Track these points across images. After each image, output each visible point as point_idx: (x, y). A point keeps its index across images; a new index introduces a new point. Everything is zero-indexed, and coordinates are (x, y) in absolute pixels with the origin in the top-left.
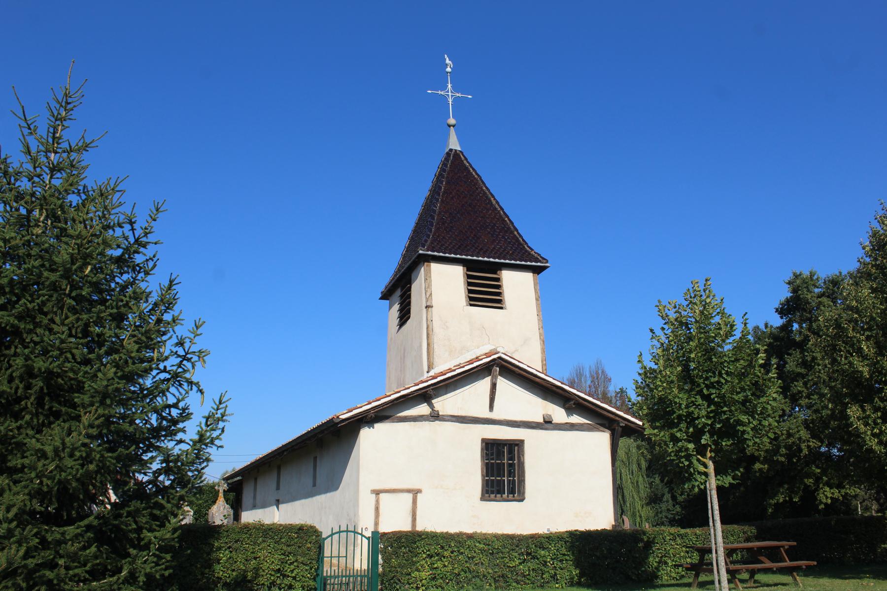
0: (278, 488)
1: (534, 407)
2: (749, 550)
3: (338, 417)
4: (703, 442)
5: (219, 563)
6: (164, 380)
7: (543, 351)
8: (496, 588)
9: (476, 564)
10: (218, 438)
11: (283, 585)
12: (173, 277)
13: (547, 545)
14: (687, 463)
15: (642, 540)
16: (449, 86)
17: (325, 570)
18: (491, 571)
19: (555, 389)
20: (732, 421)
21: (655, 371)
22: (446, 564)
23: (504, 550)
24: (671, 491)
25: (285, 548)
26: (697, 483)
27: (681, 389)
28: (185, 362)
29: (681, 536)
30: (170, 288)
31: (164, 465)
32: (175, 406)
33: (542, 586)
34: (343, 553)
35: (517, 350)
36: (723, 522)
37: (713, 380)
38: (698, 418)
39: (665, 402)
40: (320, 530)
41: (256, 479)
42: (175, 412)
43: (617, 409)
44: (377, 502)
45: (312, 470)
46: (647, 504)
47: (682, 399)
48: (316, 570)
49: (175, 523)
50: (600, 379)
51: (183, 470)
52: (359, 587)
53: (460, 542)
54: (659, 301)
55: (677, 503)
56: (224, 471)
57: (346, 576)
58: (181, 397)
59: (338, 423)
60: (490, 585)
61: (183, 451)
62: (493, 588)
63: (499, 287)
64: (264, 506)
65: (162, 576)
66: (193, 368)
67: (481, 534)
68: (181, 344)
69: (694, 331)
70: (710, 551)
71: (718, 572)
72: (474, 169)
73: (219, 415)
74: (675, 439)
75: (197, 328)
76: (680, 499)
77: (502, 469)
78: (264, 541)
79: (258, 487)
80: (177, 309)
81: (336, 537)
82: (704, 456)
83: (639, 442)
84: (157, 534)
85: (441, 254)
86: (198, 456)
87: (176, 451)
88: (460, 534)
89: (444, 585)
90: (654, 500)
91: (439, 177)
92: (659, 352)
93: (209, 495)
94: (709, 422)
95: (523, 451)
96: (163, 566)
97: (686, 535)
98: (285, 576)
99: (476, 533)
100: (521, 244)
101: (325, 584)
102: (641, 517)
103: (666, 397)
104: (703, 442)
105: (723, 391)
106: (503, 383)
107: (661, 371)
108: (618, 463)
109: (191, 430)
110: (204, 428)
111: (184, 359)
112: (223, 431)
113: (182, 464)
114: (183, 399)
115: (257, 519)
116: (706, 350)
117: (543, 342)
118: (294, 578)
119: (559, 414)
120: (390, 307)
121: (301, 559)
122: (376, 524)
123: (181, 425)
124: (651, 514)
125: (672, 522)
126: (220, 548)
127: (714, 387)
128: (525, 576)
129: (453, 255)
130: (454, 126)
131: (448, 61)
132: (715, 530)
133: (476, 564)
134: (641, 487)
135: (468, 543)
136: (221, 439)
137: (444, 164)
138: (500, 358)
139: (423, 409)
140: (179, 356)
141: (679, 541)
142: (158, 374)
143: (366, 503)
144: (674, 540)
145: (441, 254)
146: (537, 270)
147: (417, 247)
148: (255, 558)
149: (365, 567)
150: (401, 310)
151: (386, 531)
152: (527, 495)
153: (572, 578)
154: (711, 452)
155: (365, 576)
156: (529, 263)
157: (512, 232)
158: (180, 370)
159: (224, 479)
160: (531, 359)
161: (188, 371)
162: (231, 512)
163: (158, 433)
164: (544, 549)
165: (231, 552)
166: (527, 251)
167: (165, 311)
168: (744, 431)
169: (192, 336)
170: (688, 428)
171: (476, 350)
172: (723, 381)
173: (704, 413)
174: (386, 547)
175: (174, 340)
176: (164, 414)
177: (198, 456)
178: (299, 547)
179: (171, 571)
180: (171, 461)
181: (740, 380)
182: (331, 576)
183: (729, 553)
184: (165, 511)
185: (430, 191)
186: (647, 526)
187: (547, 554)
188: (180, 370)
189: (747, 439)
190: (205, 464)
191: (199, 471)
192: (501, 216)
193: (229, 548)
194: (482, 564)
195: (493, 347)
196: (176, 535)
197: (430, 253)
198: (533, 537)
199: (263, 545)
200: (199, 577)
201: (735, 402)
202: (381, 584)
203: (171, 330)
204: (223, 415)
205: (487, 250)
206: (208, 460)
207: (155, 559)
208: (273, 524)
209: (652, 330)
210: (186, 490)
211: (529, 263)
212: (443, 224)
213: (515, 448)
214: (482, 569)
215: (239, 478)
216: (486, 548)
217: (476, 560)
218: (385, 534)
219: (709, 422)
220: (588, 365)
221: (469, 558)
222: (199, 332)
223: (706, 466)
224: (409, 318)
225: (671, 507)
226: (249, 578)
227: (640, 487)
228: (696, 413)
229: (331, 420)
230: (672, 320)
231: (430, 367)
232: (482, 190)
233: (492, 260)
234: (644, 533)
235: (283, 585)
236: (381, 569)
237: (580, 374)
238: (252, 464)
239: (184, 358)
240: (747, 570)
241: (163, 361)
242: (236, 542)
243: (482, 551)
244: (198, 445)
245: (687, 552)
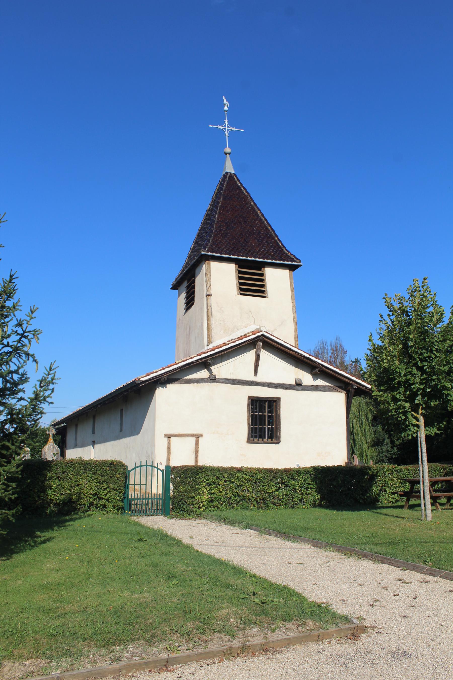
0: (94, 432)
1: (288, 373)
2: (447, 482)
3: (139, 380)
4: (417, 402)
5: (51, 489)
6: (7, 353)
7: (296, 330)
8: (258, 508)
9: (243, 491)
10: (49, 396)
11: (99, 505)
12: (12, 273)
13: (296, 477)
14: (403, 418)
15: (368, 474)
16: (226, 122)
17: (130, 494)
18: (254, 496)
19: (304, 359)
20: (439, 386)
21: (381, 347)
22: (221, 490)
23: (264, 480)
24: (390, 436)
25: (100, 478)
26: (411, 433)
27: (401, 362)
28: (23, 339)
29: (397, 471)
30: (10, 282)
31: (9, 417)
32: (16, 372)
33: (292, 507)
34: (143, 482)
35: (276, 330)
36: (429, 461)
37: (425, 355)
38: (413, 384)
39: (388, 371)
40: (126, 464)
41: (77, 426)
42: (16, 377)
43: (352, 374)
44: (169, 443)
45: (119, 419)
46: (372, 446)
47: (402, 369)
48: (124, 494)
49: (19, 460)
50: (338, 351)
51: (23, 420)
52: (156, 506)
53: (231, 474)
54: (386, 294)
55: (395, 446)
56: (53, 419)
57: (146, 499)
58: (20, 366)
59: (139, 384)
60: (254, 506)
61: (23, 407)
62: (256, 508)
63: (263, 280)
64: (83, 445)
65: (10, 499)
66: (30, 343)
67: (247, 468)
68: (20, 325)
69: (412, 316)
70: (418, 482)
71: (424, 498)
72: (244, 188)
73: (49, 379)
74: (395, 400)
75: (32, 312)
76: (397, 443)
77: (264, 420)
78: (84, 473)
79: (78, 429)
80: (16, 297)
81: (138, 470)
82: (417, 412)
83: (367, 400)
84: (6, 468)
85: (219, 255)
86: (34, 410)
87: (18, 407)
88: (231, 468)
89: (219, 506)
90: (377, 443)
91: (218, 194)
92: (385, 333)
93: (40, 437)
94: (422, 387)
95: (279, 406)
96: (11, 492)
97: (401, 470)
98: (100, 498)
99: (243, 467)
100: (280, 247)
101: (130, 505)
102: (367, 456)
103: (390, 368)
104: (417, 402)
105: (433, 364)
106: (265, 355)
107: (386, 348)
108: (351, 415)
109: (28, 390)
110: (39, 389)
111: (22, 337)
112: (53, 391)
113: (23, 416)
114: (22, 367)
115: (79, 456)
116: (422, 333)
118: (107, 500)
119: (307, 378)
120: (179, 295)
121: (112, 486)
122: (168, 460)
123: (21, 387)
124: (375, 453)
125: (391, 460)
126: (51, 478)
127: (426, 361)
128: (279, 500)
129: (227, 256)
130: (229, 154)
131: (225, 102)
132: (423, 467)
133: (243, 491)
134: (368, 433)
135: (238, 474)
136: (51, 397)
137: (222, 184)
138: (263, 335)
139: (203, 374)
140: (19, 334)
141: (395, 475)
142: (3, 348)
143: (161, 444)
144: (392, 474)
145: (219, 255)
146: (292, 268)
147: (200, 249)
148: (78, 485)
149: (160, 492)
150: (187, 298)
151: (176, 466)
152: (282, 439)
153: (315, 501)
154: (422, 409)
155: (160, 499)
156: (286, 262)
157: (273, 238)
158: (19, 345)
159: (52, 425)
160: (286, 336)
161: (26, 345)
162: (59, 450)
163: (4, 393)
164: (294, 479)
165: (60, 480)
166: (284, 253)
167: (7, 299)
168: (448, 394)
169: (28, 319)
170: (405, 391)
171: (244, 329)
172: (433, 356)
173: (418, 380)
174: (176, 478)
175: (15, 322)
176: (8, 378)
177: (34, 410)
178: (111, 477)
179: (16, 495)
180: (14, 414)
181: (446, 356)
182: (135, 499)
183: (433, 484)
184: (11, 451)
185: (211, 205)
186: (371, 463)
187: (297, 483)
188: (19, 345)
189: (450, 400)
190: (40, 416)
191: (35, 421)
192: (265, 225)
193: (58, 477)
194: (248, 490)
195: (258, 327)
196: (19, 469)
197: (210, 253)
198: (286, 471)
199: (84, 475)
200: (37, 499)
201: (441, 372)
202: (172, 505)
203: (12, 314)
204: (53, 379)
205: (254, 252)
206: (42, 413)
207: (4, 487)
208: (91, 460)
209: (381, 316)
210: (26, 435)
211: (286, 262)
212: (220, 231)
213: (273, 403)
214: (248, 494)
215: (64, 424)
216: (251, 478)
217: (244, 488)
218: (175, 468)
219: (422, 387)
220: (330, 340)
221: (238, 486)
222: (34, 315)
223: (418, 420)
224: (193, 304)
225: (389, 448)
226: (74, 500)
227: (368, 432)
228: (412, 380)
229: (134, 382)
230: (397, 309)
231: (209, 342)
232: (251, 204)
234: (370, 469)
235: (99, 505)
236: (172, 494)
237: (323, 348)
238: (73, 414)
239: (23, 336)
240: (445, 497)
241: (6, 338)
242: (63, 473)
243: (248, 481)
244: (34, 402)
245: (401, 483)
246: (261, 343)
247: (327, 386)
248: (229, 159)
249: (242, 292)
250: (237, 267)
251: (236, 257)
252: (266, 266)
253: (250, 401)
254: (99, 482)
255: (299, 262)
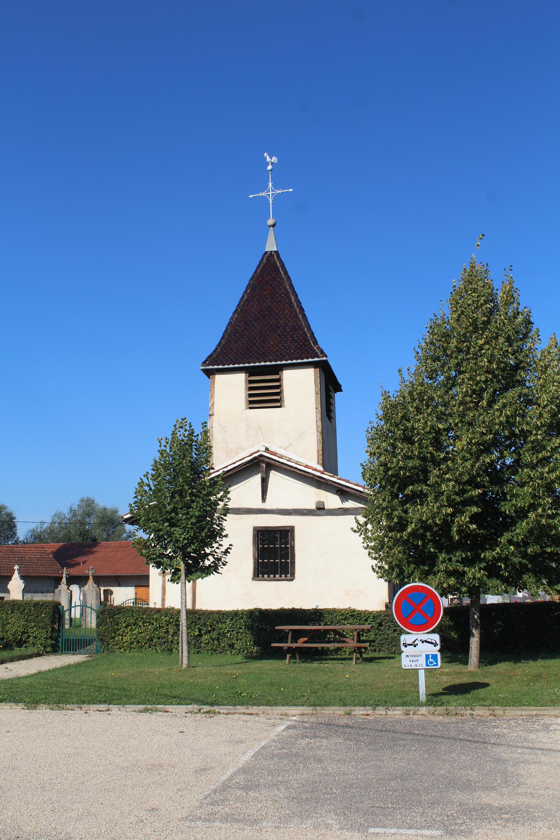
1: (308, 496)
3: (122, 517)
16: (270, 185)
117: (322, 433)
119: (333, 501)
122: (163, 600)
138: (261, 456)
164: (222, 623)
213: (286, 534)
233: (268, 363)
246: (264, 465)
247: (359, 508)
248: (273, 234)
249: (251, 406)
250: (248, 375)
254: (27, 621)
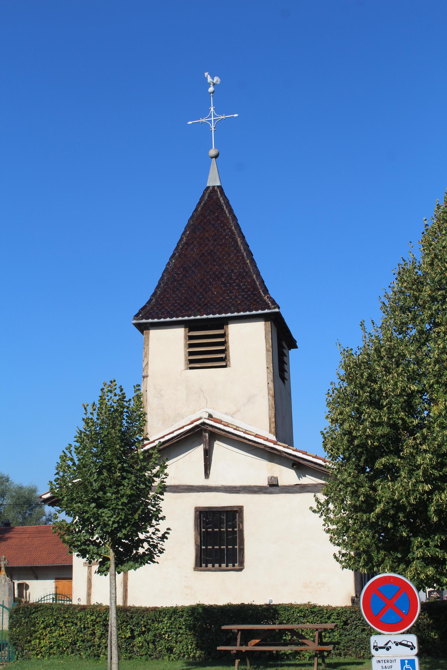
1: (260, 471)
3: (41, 497)
16: (212, 109)
117: (275, 397)
119: (287, 476)
122: (89, 595)
138: (204, 424)
152: (246, 564)
213: (234, 515)
233: (211, 316)
248: (215, 166)
250: (187, 329)
251: (186, 318)
252: (229, 322)
253: (198, 513)
255: (274, 308)
